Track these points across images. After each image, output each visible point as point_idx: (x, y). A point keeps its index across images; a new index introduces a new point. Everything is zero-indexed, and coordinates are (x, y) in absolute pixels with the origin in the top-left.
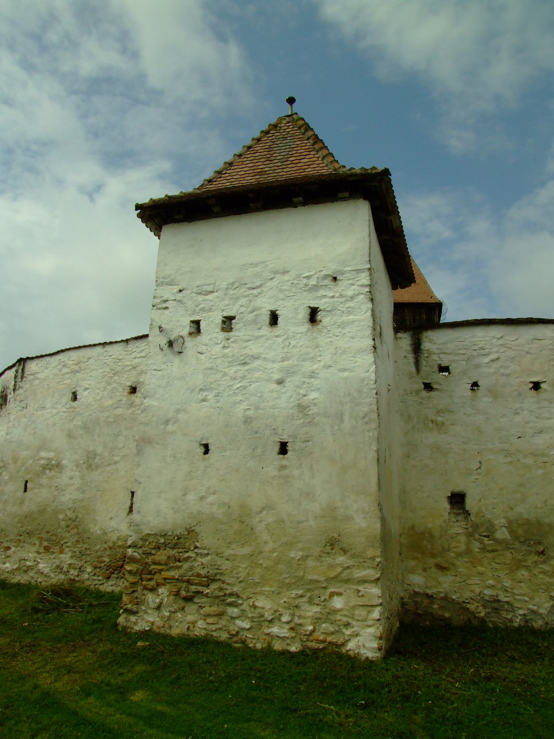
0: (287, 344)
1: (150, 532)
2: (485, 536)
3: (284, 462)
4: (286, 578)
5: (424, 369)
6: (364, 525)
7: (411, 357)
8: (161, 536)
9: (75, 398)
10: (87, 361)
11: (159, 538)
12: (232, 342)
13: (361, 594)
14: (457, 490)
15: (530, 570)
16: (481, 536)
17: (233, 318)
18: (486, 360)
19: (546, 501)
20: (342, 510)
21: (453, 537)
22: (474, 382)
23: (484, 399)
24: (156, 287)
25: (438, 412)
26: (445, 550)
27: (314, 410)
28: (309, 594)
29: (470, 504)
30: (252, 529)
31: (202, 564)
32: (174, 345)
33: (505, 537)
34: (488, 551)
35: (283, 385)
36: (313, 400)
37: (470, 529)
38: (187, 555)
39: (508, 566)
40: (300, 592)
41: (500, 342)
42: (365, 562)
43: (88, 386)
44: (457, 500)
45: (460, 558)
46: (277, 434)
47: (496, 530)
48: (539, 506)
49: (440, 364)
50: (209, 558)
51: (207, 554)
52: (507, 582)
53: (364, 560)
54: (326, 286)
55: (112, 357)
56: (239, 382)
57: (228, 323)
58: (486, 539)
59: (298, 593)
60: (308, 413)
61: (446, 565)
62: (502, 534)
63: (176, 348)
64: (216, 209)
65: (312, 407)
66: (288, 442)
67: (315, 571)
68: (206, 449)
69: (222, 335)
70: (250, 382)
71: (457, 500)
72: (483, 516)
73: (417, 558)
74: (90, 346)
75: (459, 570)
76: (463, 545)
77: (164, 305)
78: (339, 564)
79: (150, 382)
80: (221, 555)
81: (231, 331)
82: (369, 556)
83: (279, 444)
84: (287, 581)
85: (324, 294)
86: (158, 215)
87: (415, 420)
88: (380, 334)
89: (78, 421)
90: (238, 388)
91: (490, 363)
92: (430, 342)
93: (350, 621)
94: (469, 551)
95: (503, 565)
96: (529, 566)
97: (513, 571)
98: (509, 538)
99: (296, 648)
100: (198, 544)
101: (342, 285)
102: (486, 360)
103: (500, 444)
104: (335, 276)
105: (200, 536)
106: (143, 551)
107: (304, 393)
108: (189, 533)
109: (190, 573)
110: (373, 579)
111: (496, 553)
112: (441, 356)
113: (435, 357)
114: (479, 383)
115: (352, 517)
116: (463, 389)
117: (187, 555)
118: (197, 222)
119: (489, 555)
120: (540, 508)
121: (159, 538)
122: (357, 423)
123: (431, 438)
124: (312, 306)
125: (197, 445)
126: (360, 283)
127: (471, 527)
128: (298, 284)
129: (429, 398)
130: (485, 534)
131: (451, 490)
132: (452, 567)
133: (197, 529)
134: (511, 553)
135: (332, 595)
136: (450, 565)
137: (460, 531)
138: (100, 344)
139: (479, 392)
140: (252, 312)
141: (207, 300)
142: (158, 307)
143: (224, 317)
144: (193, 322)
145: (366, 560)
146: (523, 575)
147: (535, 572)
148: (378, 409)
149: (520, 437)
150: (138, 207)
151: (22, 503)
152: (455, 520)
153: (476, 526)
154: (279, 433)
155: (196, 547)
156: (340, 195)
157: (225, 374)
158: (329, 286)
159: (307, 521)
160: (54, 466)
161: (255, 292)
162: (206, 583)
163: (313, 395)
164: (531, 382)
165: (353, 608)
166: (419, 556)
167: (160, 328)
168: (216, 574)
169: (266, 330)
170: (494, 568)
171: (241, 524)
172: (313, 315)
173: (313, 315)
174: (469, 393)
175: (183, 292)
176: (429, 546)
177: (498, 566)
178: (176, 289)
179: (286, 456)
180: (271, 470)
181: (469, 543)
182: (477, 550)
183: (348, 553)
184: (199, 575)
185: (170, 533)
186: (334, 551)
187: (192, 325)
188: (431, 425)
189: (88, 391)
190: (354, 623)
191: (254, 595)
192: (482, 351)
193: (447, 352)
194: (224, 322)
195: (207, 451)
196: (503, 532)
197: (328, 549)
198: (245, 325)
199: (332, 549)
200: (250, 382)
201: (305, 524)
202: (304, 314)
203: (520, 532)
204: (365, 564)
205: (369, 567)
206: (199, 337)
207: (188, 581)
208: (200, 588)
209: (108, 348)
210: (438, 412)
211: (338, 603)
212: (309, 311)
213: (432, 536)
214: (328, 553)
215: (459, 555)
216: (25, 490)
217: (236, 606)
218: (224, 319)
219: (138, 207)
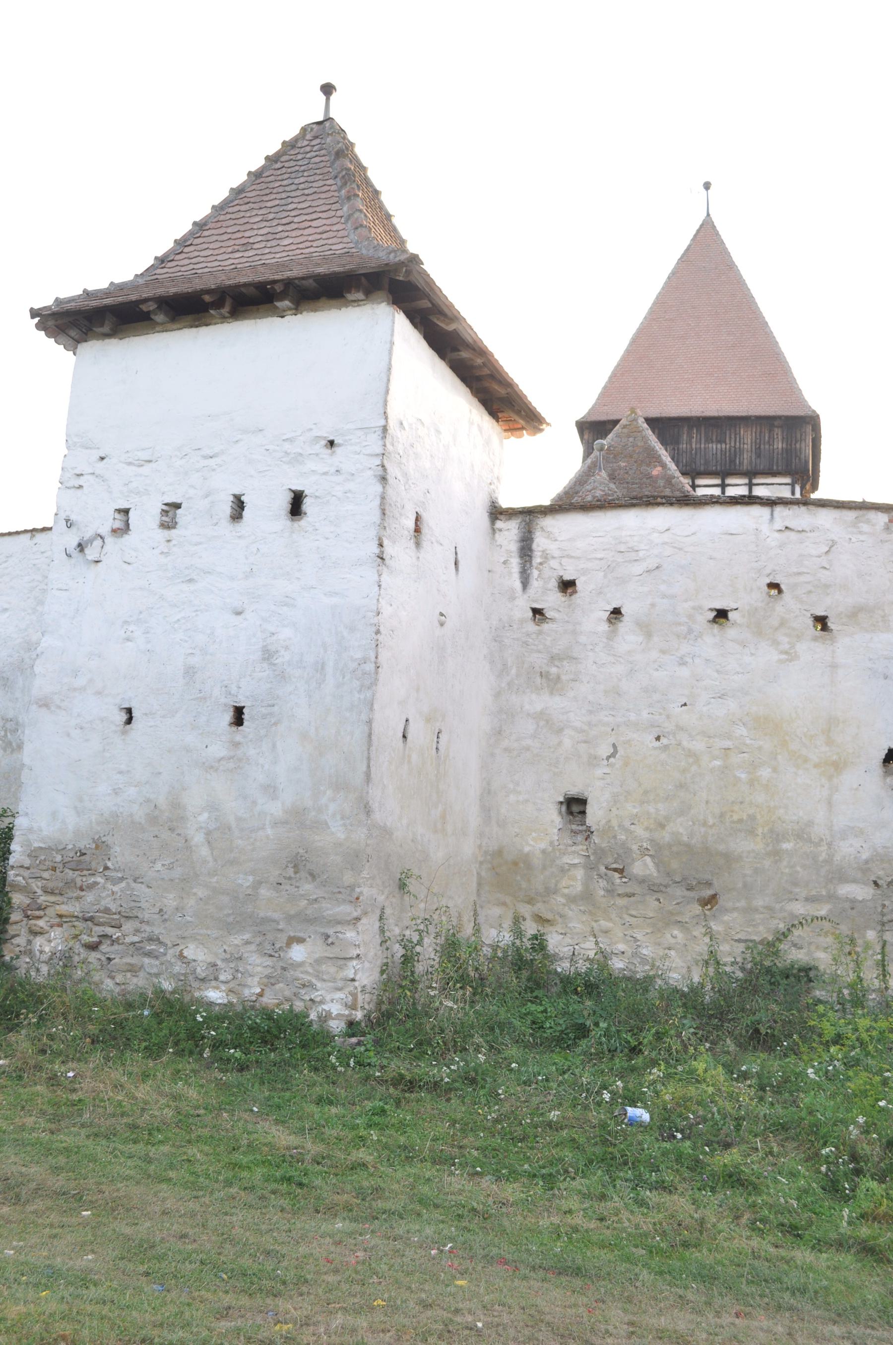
0: (255, 550)
1: (43, 845)
2: (615, 870)
3: (238, 738)
4: (229, 915)
5: (535, 584)
6: (341, 836)
7: (515, 563)
8: (58, 851)
10: (6, 562)
11: (55, 855)
12: (174, 545)
13: (330, 940)
15: (688, 929)
16: (610, 869)
17: (178, 506)
18: (638, 569)
19: (722, 815)
20: (313, 813)
21: (563, 871)
22: (615, 609)
24: (66, 452)
25: (554, 659)
26: (550, 891)
28: (258, 940)
29: (595, 814)
30: (186, 841)
31: (113, 893)
32: (87, 551)
33: (648, 872)
34: (619, 895)
35: (243, 616)
36: (285, 641)
37: (592, 858)
38: (93, 879)
39: (649, 921)
40: (247, 936)
41: (666, 537)
42: (340, 892)
43: (6, 606)
44: (575, 806)
45: (573, 906)
46: (230, 694)
47: (633, 860)
48: (711, 821)
49: (562, 577)
50: (123, 884)
51: (122, 879)
52: (647, 947)
53: (337, 890)
54: (317, 455)
55: (45, 555)
56: (180, 612)
58: (617, 875)
59: (244, 937)
60: (276, 662)
61: (549, 916)
62: (645, 867)
63: (92, 553)
65: (282, 652)
66: (244, 707)
70: (197, 611)
71: (575, 806)
72: (615, 837)
73: (504, 904)
74: (10, 534)
75: (570, 925)
76: (579, 883)
77: (77, 482)
78: (302, 896)
80: (140, 880)
81: (174, 528)
82: (346, 884)
83: (232, 709)
84: (231, 919)
85: (314, 468)
86: (80, 321)
87: (514, 671)
88: (417, 530)
90: (178, 620)
91: (645, 574)
92: (548, 537)
93: (314, 981)
94: (587, 896)
95: (642, 919)
96: (686, 923)
97: (659, 930)
98: (655, 875)
100: (109, 864)
102: (638, 569)
103: (651, 716)
104: (331, 438)
105: (112, 851)
106: (32, 873)
107: (273, 629)
108: (97, 847)
109: (96, 907)
110: (349, 918)
111: (632, 899)
112: (564, 561)
113: (553, 563)
114: (623, 611)
115: (326, 824)
116: (594, 619)
117: (93, 879)
118: (132, 338)
119: (621, 902)
120: (711, 827)
121: (55, 855)
122: (344, 678)
124: (294, 488)
125: (116, 711)
126: (368, 451)
127: (593, 854)
128: (275, 451)
129: (540, 633)
130: (614, 866)
131: (563, 791)
132: (560, 920)
133: (108, 839)
134: (658, 900)
136: (557, 917)
137: (576, 861)
138: (26, 531)
139: (620, 625)
140: (207, 496)
141: (141, 475)
142: (68, 485)
143: (166, 504)
144: (119, 511)
145: (341, 890)
146: (675, 937)
147: (695, 933)
148: (376, 658)
149: (685, 705)
152: (570, 842)
153: (600, 853)
154: (232, 692)
155: (106, 868)
156: (350, 297)
157: (162, 597)
158: (321, 456)
159: (263, 828)
161: (212, 462)
162: (118, 922)
163: (286, 633)
164: (711, 610)
165: (319, 961)
166: (508, 900)
167: (67, 521)
168: (131, 909)
169: (226, 527)
170: (627, 924)
174: (605, 627)
175: (105, 461)
176: (524, 885)
177: (633, 921)
179: (240, 728)
180: (217, 750)
181: (587, 880)
182: (602, 893)
183: (318, 880)
184: (107, 911)
185: (70, 847)
186: (298, 876)
187: (117, 516)
188: (538, 680)
189: (7, 614)
190: (319, 985)
191: (182, 940)
192: (633, 554)
193: (573, 555)
194: (164, 512)
195: (129, 721)
196: (645, 865)
197: (290, 872)
198: (195, 519)
199: (296, 873)
200: (197, 611)
201: (261, 833)
202: (284, 501)
203: (675, 865)
204: (340, 896)
205: (344, 901)
206: (126, 537)
207: (91, 919)
208: (109, 931)
209: (39, 537)
211: (298, 953)
212: (289, 497)
213: (529, 866)
214: (290, 878)
215: (572, 900)
217: (157, 957)
218: (165, 508)
219: (34, 313)
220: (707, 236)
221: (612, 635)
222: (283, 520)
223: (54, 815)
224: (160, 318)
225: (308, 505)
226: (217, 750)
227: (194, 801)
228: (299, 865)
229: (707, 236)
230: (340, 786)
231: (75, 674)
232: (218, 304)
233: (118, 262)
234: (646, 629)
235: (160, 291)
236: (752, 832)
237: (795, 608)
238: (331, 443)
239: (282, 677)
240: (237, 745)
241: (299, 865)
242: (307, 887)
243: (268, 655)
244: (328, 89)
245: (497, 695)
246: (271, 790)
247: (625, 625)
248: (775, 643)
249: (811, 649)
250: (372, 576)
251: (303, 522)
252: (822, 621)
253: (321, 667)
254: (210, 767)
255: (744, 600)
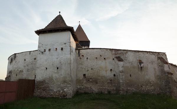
9: (25, 60)
14: (84, 74)
17: (50, 49)
18: (89, 54)
23: (88, 60)
25: (82, 62)
26: (82, 83)
27: (62, 63)
44: (84, 75)
57: (50, 50)
64: (11, 67)
67: (62, 85)
68: (47, 68)
69: (49, 52)
71: (84, 75)
79: (38, 59)
86: (39, 32)
89: (26, 64)
94: (86, 83)
99: (128, 54)
101: (66, 45)
102: (89, 54)
116: (86, 59)
123: (81, 66)
135: (64, 89)
150: (35, 31)
151: (16, 78)
160: (21, 71)
163: (62, 60)
165: (67, 90)
171: (51, 79)
172: (62, 49)
173: (62, 49)
174: (86, 59)
178: (42, 44)
184: (45, 87)
202: (61, 49)
210: (82, 62)
211: (65, 90)
215: (85, 83)
216: (17, 75)
219: (35, 31)
220: (80, 25)
221: (87, 60)
222: (61, 51)
223: (39, 78)
224: (48, 32)
225: (63, 49)
226: (56, 71)
227: (54, 76)
228: (65, 82)
229: (80, 25)
230: (68, 74)
231: (41, 65)
232: (54, 31)
233: (43, 26)
234: (90, 60)
235: (48, 30)
236: (100, 77)
237: (102, 57)
238: (65, 44)
239: (62, 65)
240: (58, 71)
241: (65, 82)
242: (66, 84)
243: (60, 63)
244: (60, 12)
245: (77, 66)
246: (61, 75)
247: (88, 59)
248: (101, 60)
249: (104, 61)
250: (70, 56)
251: (63, 51)
252: (105, 59)
253: (65, 64)
254: (55, 73)
255: (99, 57)
